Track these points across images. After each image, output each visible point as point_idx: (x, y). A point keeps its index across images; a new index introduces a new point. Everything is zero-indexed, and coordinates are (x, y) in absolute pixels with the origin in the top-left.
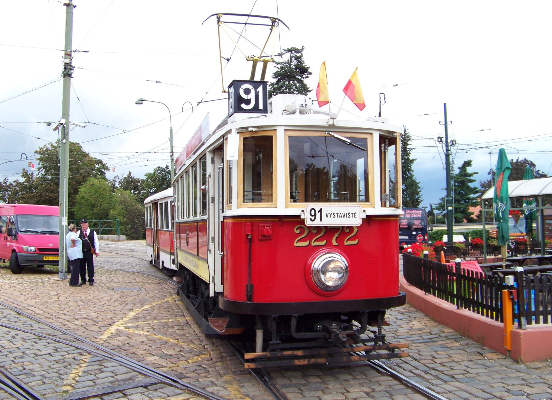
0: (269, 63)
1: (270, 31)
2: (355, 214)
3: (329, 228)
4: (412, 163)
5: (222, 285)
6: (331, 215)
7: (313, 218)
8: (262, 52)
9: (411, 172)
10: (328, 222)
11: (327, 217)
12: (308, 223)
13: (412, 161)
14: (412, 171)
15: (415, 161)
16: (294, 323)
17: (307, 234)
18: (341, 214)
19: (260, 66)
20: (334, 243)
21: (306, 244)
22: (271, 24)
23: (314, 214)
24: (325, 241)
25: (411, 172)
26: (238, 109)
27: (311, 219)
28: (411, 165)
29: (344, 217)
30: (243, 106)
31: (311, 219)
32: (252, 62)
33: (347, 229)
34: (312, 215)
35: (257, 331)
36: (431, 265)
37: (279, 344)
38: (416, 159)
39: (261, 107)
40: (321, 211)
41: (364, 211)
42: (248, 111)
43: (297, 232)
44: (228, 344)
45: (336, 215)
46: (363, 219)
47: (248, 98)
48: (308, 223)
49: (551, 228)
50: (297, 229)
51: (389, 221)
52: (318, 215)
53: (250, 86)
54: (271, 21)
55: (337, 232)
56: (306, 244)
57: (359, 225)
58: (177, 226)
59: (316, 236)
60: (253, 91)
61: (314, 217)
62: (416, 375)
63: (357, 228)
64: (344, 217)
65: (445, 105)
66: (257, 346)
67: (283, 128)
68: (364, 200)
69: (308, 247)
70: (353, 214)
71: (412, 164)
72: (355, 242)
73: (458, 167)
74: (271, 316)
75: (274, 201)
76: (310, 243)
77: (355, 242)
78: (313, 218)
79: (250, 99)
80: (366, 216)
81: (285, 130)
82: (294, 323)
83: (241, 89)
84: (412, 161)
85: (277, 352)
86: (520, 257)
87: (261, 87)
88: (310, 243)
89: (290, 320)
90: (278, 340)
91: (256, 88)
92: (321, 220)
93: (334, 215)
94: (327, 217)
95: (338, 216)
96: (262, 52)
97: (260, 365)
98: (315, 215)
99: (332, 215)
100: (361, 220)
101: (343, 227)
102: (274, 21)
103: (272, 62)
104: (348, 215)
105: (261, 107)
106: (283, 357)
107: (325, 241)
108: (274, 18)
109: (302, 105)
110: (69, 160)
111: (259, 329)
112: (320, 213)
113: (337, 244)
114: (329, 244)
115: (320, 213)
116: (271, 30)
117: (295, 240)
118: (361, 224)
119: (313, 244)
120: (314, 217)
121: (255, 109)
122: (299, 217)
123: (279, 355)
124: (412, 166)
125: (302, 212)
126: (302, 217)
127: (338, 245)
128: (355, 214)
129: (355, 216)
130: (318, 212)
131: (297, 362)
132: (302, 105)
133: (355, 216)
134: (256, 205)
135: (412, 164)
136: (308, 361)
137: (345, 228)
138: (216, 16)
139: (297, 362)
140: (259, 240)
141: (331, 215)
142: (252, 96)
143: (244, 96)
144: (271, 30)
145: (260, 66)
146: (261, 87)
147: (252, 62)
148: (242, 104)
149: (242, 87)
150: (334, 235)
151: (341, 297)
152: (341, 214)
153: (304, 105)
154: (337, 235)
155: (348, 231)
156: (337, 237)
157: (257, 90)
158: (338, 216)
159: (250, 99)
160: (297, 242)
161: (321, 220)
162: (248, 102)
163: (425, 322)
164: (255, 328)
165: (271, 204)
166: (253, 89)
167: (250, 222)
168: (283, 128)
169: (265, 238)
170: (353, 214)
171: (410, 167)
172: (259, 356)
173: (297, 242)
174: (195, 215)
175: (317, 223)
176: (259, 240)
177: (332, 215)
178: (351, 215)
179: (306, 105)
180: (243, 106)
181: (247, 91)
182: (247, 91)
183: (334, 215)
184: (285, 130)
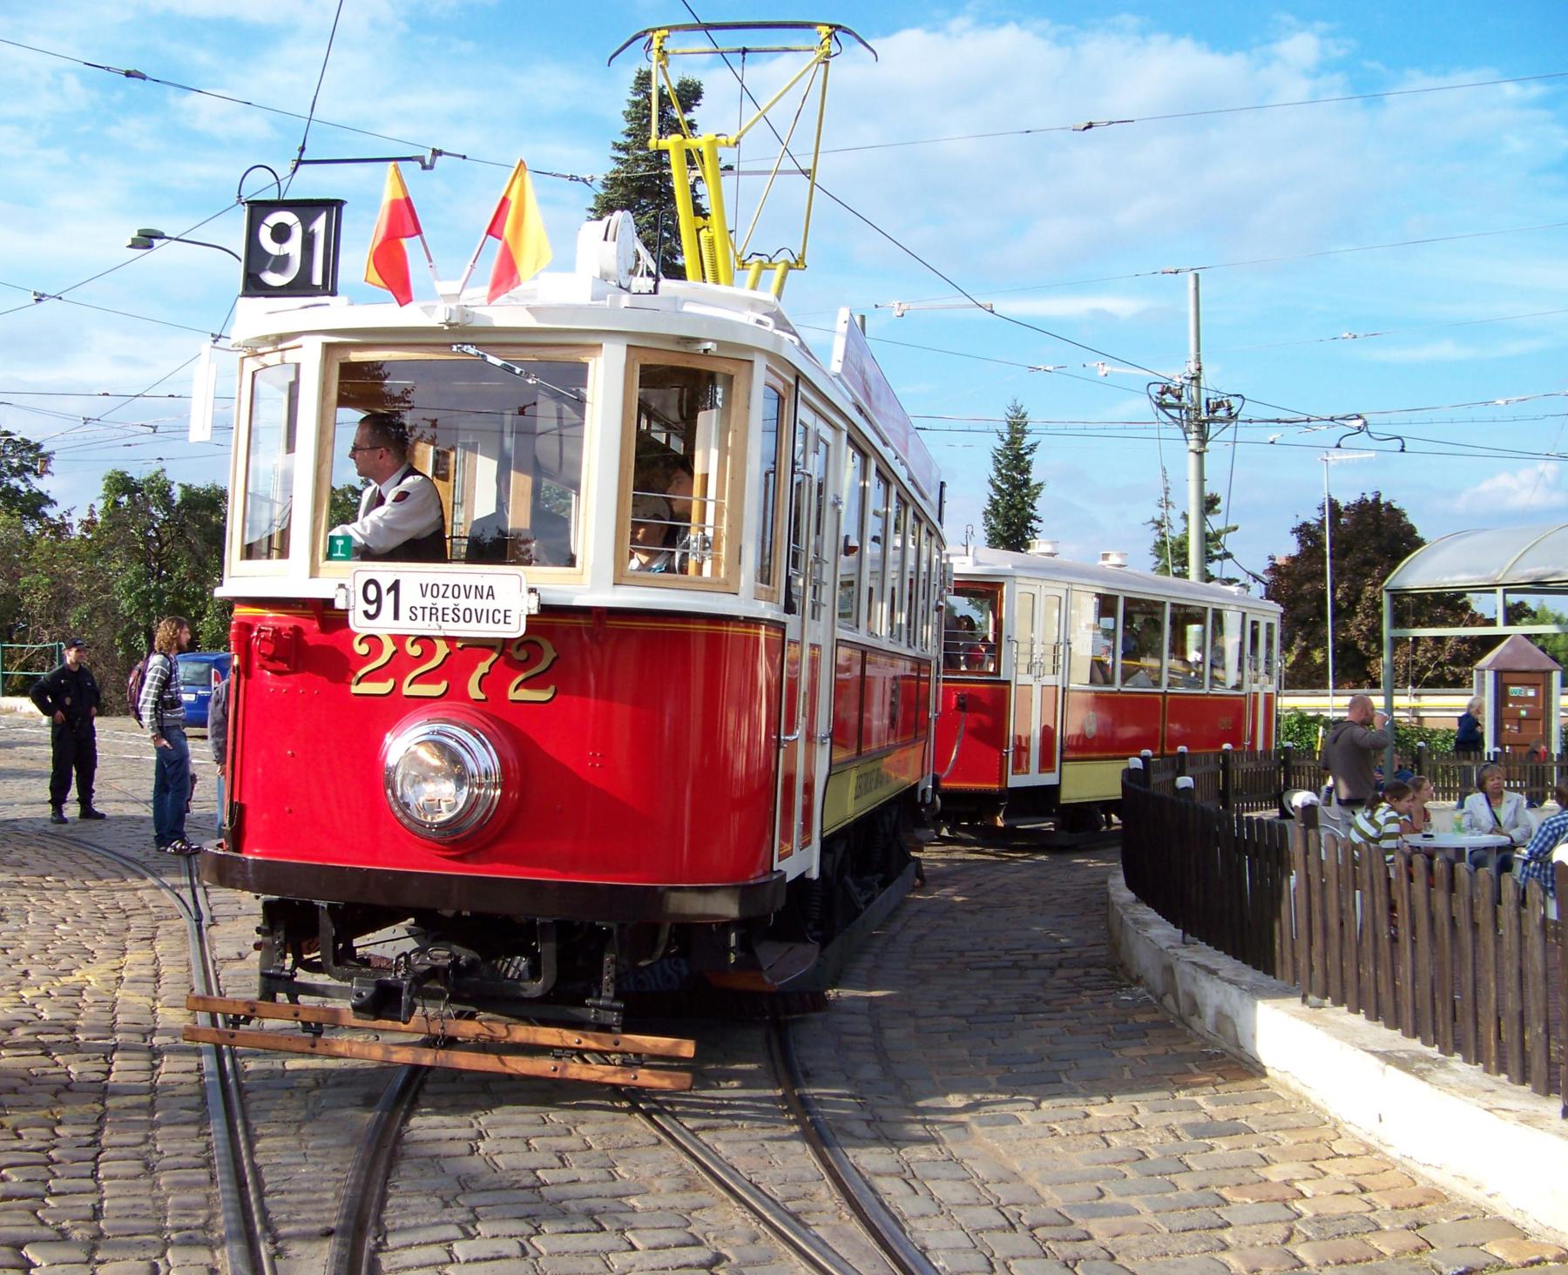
7: (372, 609)
20: (475, 692)
21: (383, 688)
23: (374, 595)
24: (444, 685)
26: (254, 286)
27: (366, 613)
30: (272, 279)
31: (366, 613)
39: (317, 279)
40: (395, 587)
42: (279, 292)
49: (1523, 713)
51: (685, 637)
52: (388, 600)
55: (484, 658)
56: (383, 688)
58: (925, 671)
68: (463, 557)
73: (1297, 524)
76: (397, 687)
78: (372, 609)
79: (287, 256)
87: (322, 219)
88: (397, 687)
91: (306, 222)
92: (396, 617)
98: (379, 600)
105: (317, 279)
107: (444, 685)
110: (630, 519)
112: (393, 593)
115: (393, 593)
117: (511, 680)
119: (407, 690)
121: (301, 287)
127: (486, 700)
130: (389, 591)
142: (293, 247)
143: (271, 247)
146: (322, 219)
149: (267, 221)
155: (415, 651)
156: (484, 675)
160: (410, 684)
161: (396, 617)
162: (281, 264)
163: (962, 960)
173: (410, 684)
180: (272, 279)
181: (281, 233)
182: (281, 233)
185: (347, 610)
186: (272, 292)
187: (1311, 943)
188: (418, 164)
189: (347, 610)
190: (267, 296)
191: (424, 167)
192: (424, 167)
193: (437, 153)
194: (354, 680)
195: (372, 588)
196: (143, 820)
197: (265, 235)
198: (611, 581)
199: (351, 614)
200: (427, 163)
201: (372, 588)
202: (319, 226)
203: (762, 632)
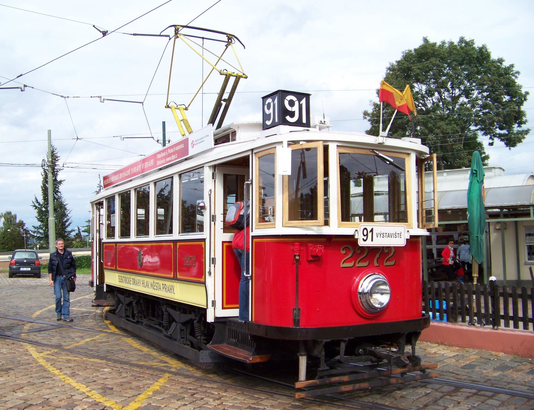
0: (241, 79)
1: (226, 47)
2: (401, 234)
3: (371, 249)
4: (60, 184)
5: (212, 306)
6: (380, 235)
7: (365, 238)
8: (214, 68)
9: (59, 194)
10: (378, 242)
11: (377, 237)
12: (361, 243)
13: (60, 182)
14: (60, 192)
15: (63, 182)
16: (343, 346)
17: (367, 255)
18: (389, 234)
19: (232, 80)
20: (376, 264)
21: (350, 265)
22: (227, 41)
25: (59, 194)
27: (363, 239)
28: (59, 186)
29: (391, 237)
30: (288, 118)
31: (363, 239)
32: (225, 76)
33: (386, 249)
34: (364, 235)
35: (300, 358)
36: (459, 285)
37: (327, 370)
38: (64, 180)
39: (304, 121)
40: (372, 231)
41: (408, 231)
43: (343, 252)
44: (508, 389)
45: (385, 235)
46: (407, 239)
47: (293, 111)
48: (361, 243)
50: (343, 250)
52: (370, 235)
53: (294, 98)
54: (227, 38)
55: (378, 253)
56: (350, 265)
57: (404, 246)
59: (361, 256)
60: (297, 103)
61: (366, 237)
62: (115, 367)
63: (394, 249)
64: (391, 237)
65: (276, 134)
66: (300, 373)
67: (335, 144)
69: (353, 268)
70: (399, 234)
71: (60, 186)
72: (392, 263)
74: (323, 341)
75: (318, 219)
77: (392, 263)
80: (409, 236)
81: (338, 146)
82: (343, 346)
83: (285, 100)
84: (60, 182)
85: (325, 379)
86: (475, 275)
87: (304, 99)
89: (339, 345)
90: (325, 366)
91: (299, 100)
92: (372, 240)
93: (382, 235)
94: (377, 237)
95: (387, 237)
96: (214, 68)
97: (310, 394)
98: (367, 235)
99: (382, 235)
100: (406, 240)
101: (383, 247)
102: (230, 38)
103: (245, 78)
104: (395, 236)
105: (304, 121)
106: (331, 384)
108: (230, 35)
109: (321, 121)
111: (302, 355)
112: (371, 232)
113: (378, 265)
114: (371, 264)
115: (371, 232)
116: (227, 46)
118: (405, 244)
119: (357, 265)
120: (366, 237)
121: (299, 123)
122: (352, 236)
123: (327, 382)
124: (59, 188)
125: (356, 232)
126: (356, 237)
127: (379, 266)
128: (401, 234)
129: (401, 237)
130: (370, 232)
131: (344, 388)
132: (321, 121)
133: (401, 237)
134: (300, 223)
135: (60, 186)
136: (353, 387)
137: (385, 248)
138: (173, 28)
139: (344, 388)
140: (308, 261)
141: (380, 235)
142: (296, 109)
144: (227, 46)
145: (232, 80)
146: (304, 99)
147: (225, 76)
148: (287, 116)
150: (375, 256)
151: (386, 319)
152: (389, 234)
153: (323, 122)
154: (378, 256)
155: (386, 251)
156: (378, 258)
157: (301, 103)
158: (387, 237)
159: (294, 112)
161: (372, 240)
162: (292, 114)
164: (298, 354)
165: (316, 222)
166: (297, 101)
167: (299, 242)
168: (335, 144)
169: (316, 259)
170: (399, 234)
171: (58, 188)
172: (310, 384)
174: (125, 232)
175: (369, 243)
176: (308, 261)
177: (382, 235)
178: (397, 235)
179: (325, 122)
180: (288, 118)
181: (292, 103)
182: (292, 103)
183: (382, 235)
184: (338, 146)
185: (358, 239)
186: (291, 124)
187: (360, 310)
188: (20, 90)
189: (358, 239)
190: (289, 125)
191: (22, 91)
192: (22, 91)
193: (25, 86)
194: (342, 262)
195: (365, 231)
196: (432, 322)
197: (286, 103)
198: (337, 226)
199: (359, 240)
200: (23, 89)
201: (365, 231)
202: (303, 102)
203: (420, 239)
